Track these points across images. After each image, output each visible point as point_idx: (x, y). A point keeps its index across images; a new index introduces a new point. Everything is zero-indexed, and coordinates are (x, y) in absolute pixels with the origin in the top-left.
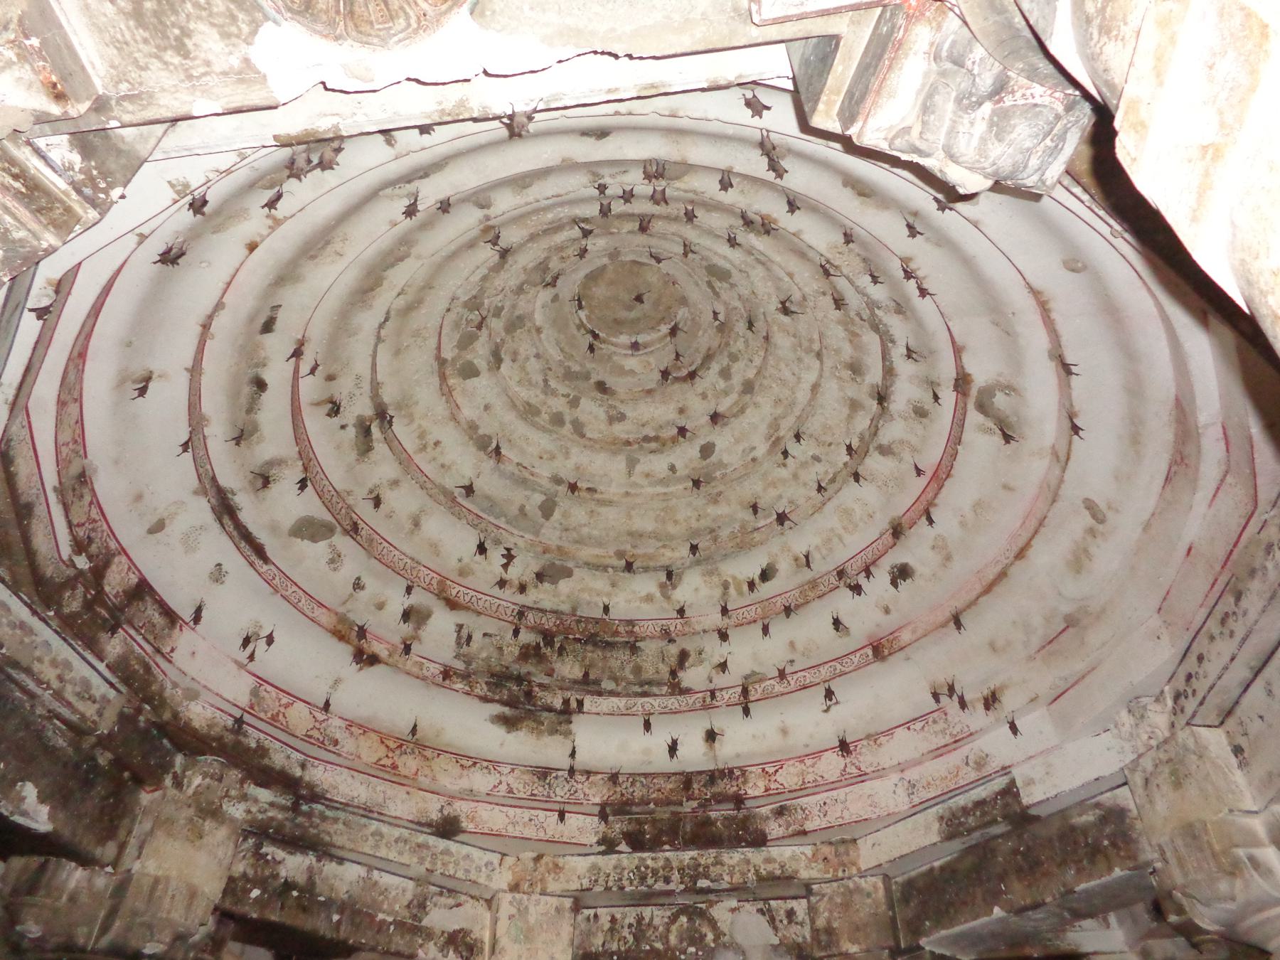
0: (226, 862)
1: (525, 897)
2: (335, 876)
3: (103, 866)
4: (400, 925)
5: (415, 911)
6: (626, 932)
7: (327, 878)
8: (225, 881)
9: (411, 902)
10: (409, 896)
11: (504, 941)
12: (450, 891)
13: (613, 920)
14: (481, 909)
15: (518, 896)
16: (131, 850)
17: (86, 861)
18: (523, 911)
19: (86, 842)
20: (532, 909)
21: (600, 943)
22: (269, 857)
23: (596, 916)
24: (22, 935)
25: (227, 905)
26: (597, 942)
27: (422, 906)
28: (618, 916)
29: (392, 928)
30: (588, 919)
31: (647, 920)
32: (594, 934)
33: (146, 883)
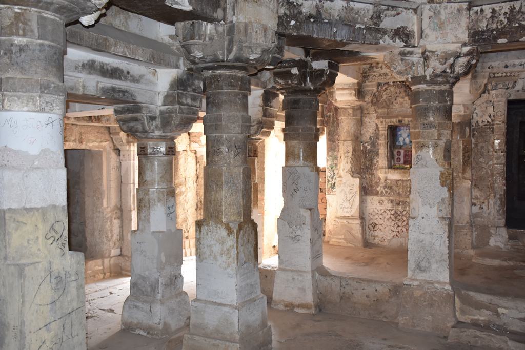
0: (275, 10)
1: (438, 5)
2: (331, 8)
3: (219, 21)
4: (368, 29)
5: (375, 21)
6: (502, 18)
7: (327, 10)
8: (277, 19)
9: (372, 16)
10: (371, 13)
11: (427, 31)
12: (393, 7)
13: (494, 11)
14: (410, 14)
15: (433, 5)
16: (229, 10)
17: (211, 20)
18: (437, 13)
19: (208, 11)
20: (442, 11)
21: (485, 25)
22: (295, 3)
23: (482, 10)
24: (195, 57)
25: (280, 30)
26: (483, 25)
27: (379, 17)
28: (497, 9)
29: (365, 31)
30: (477, 13)
31: (517, 9)
32: (481, 21)
33: (242, 27)
